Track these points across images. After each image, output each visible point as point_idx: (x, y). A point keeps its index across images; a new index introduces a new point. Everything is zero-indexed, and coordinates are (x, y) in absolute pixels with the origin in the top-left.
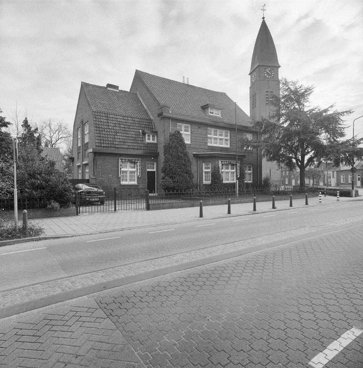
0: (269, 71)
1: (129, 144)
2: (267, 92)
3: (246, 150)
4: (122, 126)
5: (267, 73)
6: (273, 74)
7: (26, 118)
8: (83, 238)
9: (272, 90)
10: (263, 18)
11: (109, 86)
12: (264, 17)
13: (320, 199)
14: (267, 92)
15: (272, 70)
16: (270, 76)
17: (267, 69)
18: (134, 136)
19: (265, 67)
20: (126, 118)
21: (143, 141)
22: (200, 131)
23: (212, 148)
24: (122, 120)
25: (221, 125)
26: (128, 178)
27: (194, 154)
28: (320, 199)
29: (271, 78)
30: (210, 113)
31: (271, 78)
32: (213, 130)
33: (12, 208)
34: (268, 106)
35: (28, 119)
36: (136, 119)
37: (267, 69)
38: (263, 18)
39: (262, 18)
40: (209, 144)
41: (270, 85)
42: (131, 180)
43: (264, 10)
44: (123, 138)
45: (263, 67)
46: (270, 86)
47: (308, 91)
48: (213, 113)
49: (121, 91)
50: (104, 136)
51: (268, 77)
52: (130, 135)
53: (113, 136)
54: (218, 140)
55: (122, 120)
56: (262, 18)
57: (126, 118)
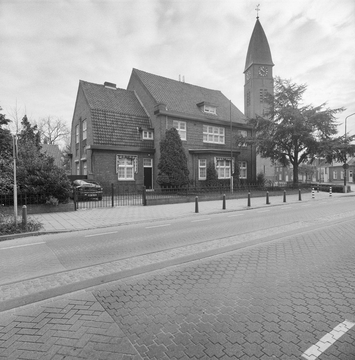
0: (263, 69)
1: (126, 141)
2: (261, 90)
3: (241, 147)
4: (119, 123)
5: (261, 71)
6: (267, 73)
7: (25, 116)
8: (81, 232)
9: (266, 88)
10: (258, 18)
11: (107, 84)
12: (258, 16)
13: (313, 195)
14: (261, 90)
15: (266, 68)
16: (264, 75)
17: (261, 68)
18: (131, 133)
19: (259, 66)
20: (123, 116)
21: (140, 138)
22: (195, 128)
23: (208, 145)
24: (119, 118)
25: (216, 122)
26: (125, 174)
27: (190, 151)
28: (313, 195)
29: (265, 76)
30: (206, 110)
31: (265, 76)
32: (208, 127)
33: (12, 203)
34: (262, 104)
35: (27, 117)
36: (133, 117)
37: (261, 68)
38: (258, 18)
39: (257, 18)
40: (204, 141)
41: (264, 83)
42: (128, 176)
43: (258, 10)
44: (121, 135)
45: (257, 66)
46: (264, 84)
47: (301, 89)
48: (208, 111)
49: (119, 89)
50: (102, 133)
51: (262, 75)
52: (127, 133)
53: (110, 133)
54: (213, 137)
55: (119, 118)
56: (257, 18)
57: (123, 116)
